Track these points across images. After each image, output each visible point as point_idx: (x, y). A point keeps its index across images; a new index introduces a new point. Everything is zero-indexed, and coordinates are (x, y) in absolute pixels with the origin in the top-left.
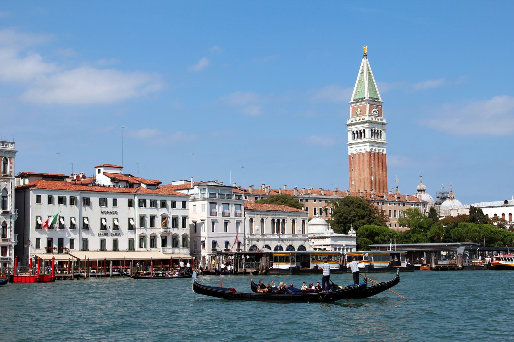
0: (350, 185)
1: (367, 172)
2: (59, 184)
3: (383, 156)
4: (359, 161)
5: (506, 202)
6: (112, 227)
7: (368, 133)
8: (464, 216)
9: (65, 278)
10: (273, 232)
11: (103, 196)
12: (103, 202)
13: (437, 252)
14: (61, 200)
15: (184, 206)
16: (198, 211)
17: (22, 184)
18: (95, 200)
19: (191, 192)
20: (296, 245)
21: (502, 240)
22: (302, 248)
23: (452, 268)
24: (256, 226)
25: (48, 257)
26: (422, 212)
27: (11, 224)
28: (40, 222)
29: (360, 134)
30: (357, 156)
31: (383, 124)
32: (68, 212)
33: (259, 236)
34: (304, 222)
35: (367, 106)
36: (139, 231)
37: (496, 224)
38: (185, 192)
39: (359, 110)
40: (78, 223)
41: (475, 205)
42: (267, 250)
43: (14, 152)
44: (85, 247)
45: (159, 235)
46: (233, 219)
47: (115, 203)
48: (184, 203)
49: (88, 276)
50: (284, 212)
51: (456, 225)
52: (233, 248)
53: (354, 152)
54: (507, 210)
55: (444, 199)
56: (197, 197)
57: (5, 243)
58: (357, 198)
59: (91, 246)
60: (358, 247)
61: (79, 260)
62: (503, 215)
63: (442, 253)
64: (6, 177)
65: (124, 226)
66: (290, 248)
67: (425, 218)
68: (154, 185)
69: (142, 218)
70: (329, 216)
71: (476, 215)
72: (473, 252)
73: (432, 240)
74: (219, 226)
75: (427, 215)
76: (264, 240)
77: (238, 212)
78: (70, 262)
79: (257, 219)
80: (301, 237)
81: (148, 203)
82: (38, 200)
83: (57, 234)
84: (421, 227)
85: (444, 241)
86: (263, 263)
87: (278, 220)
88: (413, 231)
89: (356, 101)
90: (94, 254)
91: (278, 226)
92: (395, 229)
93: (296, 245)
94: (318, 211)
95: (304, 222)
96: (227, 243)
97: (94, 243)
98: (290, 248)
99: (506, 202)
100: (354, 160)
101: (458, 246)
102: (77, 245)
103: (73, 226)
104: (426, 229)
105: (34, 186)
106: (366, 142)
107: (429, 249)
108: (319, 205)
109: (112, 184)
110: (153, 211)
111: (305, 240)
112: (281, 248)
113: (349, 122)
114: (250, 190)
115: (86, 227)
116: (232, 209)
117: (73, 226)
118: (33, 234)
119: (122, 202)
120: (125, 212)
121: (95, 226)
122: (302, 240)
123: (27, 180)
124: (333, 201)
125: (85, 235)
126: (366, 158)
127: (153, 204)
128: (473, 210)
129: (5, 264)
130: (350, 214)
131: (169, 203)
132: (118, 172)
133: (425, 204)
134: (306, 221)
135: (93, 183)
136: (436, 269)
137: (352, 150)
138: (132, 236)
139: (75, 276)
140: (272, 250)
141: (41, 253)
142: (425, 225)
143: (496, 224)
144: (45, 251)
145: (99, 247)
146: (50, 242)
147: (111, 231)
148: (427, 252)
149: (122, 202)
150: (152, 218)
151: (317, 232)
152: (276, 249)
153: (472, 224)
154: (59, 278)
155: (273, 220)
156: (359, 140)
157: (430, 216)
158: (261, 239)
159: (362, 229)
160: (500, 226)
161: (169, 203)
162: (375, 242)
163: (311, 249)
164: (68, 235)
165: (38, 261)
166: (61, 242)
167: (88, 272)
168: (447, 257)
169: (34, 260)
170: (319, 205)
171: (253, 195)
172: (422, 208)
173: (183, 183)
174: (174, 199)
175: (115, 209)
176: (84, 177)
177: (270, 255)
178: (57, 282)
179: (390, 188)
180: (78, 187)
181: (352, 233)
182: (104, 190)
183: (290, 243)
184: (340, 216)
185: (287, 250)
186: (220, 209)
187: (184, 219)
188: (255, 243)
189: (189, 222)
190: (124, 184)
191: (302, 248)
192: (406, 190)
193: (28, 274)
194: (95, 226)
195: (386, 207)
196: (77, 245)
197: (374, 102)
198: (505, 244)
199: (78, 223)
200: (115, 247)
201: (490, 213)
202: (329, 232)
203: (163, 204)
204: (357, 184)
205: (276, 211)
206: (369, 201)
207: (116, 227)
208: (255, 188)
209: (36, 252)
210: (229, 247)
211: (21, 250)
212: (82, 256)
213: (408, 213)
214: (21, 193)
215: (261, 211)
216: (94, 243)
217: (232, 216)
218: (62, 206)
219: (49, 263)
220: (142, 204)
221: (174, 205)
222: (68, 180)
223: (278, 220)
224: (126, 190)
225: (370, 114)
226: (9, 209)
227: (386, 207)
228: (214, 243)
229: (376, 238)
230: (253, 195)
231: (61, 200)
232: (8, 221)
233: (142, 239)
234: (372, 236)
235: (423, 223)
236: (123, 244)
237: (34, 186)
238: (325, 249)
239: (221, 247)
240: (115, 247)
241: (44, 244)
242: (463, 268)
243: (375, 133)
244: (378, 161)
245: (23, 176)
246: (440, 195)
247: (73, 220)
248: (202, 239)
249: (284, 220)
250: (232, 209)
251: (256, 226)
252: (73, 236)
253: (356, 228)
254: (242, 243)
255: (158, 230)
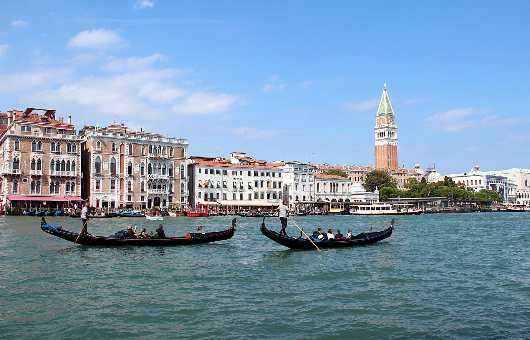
0: (376, 164)
1: (386, 156)
2: (210, 163)
3: (188, 166)
4: (381, 150)
5: (465, 174)
6: (239, 187)
7: (387, 133)
8: (441, 182)
9: (214, 215)
10: (331, 191)
11: (235, 170)
12: (234, 173)
13: (425, 203)
14: (212, 172)
15: (280, 176)
16: (287, 178)
17: (191, 163)
18: (230, 172)
19: (284, 167)
20: (344, 198)
21: (463, 196)
22: (348, 200)
23: (434, 212)
24: (321, 187)
25: (205, 203)
26: (417, 180)
27: (186, 184)
28: (200, 184)
29: (382, 134)
30: (380, 147)
31: (395, 128)
32: (215, 178)
33: (323, 193)
34: (349, 185)
35: (386, 118)
36: (255, 189)
37: (459, 187)
38: (280, 167)
39: (381, 120)
40: (221, 185)
41: (448, 176)
42: (327, 201)
43: (187, 145)
44: (225, 198)
45: (265, 192)
46: (308, 184)
47: (241, 174)
48: (280, 174)
49: (226, 214)
50: (337, 179)
51: (437, 187)
52: (308, 200)
53: (378, 145)
54: (466, 179)
55: (430, 172)
56: (287, 170)
57: (183, 195)
58: (380, 171)
59: (244, 198)
60: (380, 200)
61: (221, 205)
62: (464, 181)
63: (428, 203)
64: (183, 158)
65: (246, 187)
66: (341, 200)
67: (419, 183)
68: (263, 164)
69: (256, 182)
70: (364, 182)
71: (448, 181)
72: (446, 203)
73: (423, 196)
74: (300, 187)
75: (420, 181)
76: (326, 195)
77: (311, 179)
78: (217, 206)
79: (322, 183)
80: (347, 194)
81: (259, 173)
82: (200, 172)
83: (209, 191)
84: (417, 189)
85: (429, 197)
86: (325, 208)
87: (334, 184)
88: (412, 191)
89: (380, 115)
90: (230, 202)
91: (334, 187)
92: (402, 190)
93: (344, 198)
94: (357, 179)
95: (349, 185)
96: (304, 197)
97: (230, 196)
98: (341, 200)
99: (465, 174)
100: (378, 150)
101: (438, 199)
102: (221, 197)
103: (218, 186)
104: (420, 190)
105: (198, 164)
106: (386, 139)
107: (421, 201)
108: (358, 175)
109: (239, 163)
110: (263, 178)
111: (349, 196)
112: (336, 200)
113: (376, 127)
114: (318, 167)
115: (225, 187)
116: (307, 178)
117: (218, 186)
118: (197, 190)
119: (245, 173)
120: (246, 179)
121: (230, 186)
122: (347, 195)
123: (194, 160)
124: (366, 173)
125: (225, 191)
126: (386, 148)
127: (262, 174)
128: (446, 178)
129: (183, 206)
130: (377, 181)
131: (271, 174)
132: (243, 156)
133: (419, 175)
134: (350, 185)
135: (229, 162)
136: (425, 213)
137: (377, 144)
138: (251, 192)
139: (219, 214)
140: (330, 202)
141: (201, 201)
142: (419, 188)
143: (459, 187)
144: (203, 200)
145: (232, 198)
146: (206, 195)
147: (239, 189)
148: (420, 203)
149: (245, 173)
150: (262, 182)
151: (356, 190)
152: (332, 201)
153: (446, 187)
154: (211, 215)
155: (331, 184)
156: (382, 138)
157: (422, 182)
158: (324, 195)
159: (382, 189)
160: (461, 188)
161: (271, 174)
162: (390, 197)
163: (353, 201)
164: (215, 191)
165: (200, 205)
166: (212, 194)
167: (226, 212)
168: (431, 206)
169: (198, 205)
170: (358, 175)
171: (320, 169)
172: (417, 178)
173: (279, 162)
174: (274, 171)
175: (241, 177)
176: (224, 159)
177: (329, 204)
178: (209, 217)
179: (399, 166)
180: (221, 165)
181: (377, 191)
182: (235, 166)
183: (341, 197)
184: (370, 182)
185: (339, 201)
186: (300, 177)
187: (280, 183)
188: (320, 197)
189: (282, 185)
190: (246, 163)
191: (348, 200)
192: (409, 167)
193: (194, 212)
194: (230, 186)
195: (397, 177)
196: (221, 197)
197: (390, 115)
198: (464, 198)
199: (221, 185)
200: (241, 199)
201: (456, 180)
202: (364, 191)
203: (268, 174)
204: (381, 164)
205: (333, 179)
206: (387, 174)
207: (241, 187)
208: (320, 166)
209: (199, 200)
210: (312, 199)
211: (191, 199)
212: (223, 203)
213: (409, 181)
214: (191, 167)
215: (324, 178)
216: (230, 196)
217: (307, 181)
218: (212, 175)
219: (205, 207)
220: (256, 174)
221: (274, 175)
222: (216, 161)
223: (334, 184)
224: (247, 166)
225: (388, 123)
226: (184, 177)
227: (397, 177)
228: (297, 197)
229: (391, 195)
230: (320, 169)
231: (212, 172)
232: (184, 183)
233: (256, 194)
234: (388, 193)
235: (418, 186)
236: (246, 197)
237: (198, 164)
238: (361, 201)
239: (301, 199)
240: (241, 199)
241: (203, 196)
242: (440, 212)
243: (390, 134)
244: (392, 150)
245: (191, 158)
246: (428, 170)
247: (235, 184)
248: (290, 195)
249: (337, 184)
250: (307, 178)
251: (321, 187)
252: (218, 192)
253: (379, 189)
254: (313, 197)
255: (265, 189)
